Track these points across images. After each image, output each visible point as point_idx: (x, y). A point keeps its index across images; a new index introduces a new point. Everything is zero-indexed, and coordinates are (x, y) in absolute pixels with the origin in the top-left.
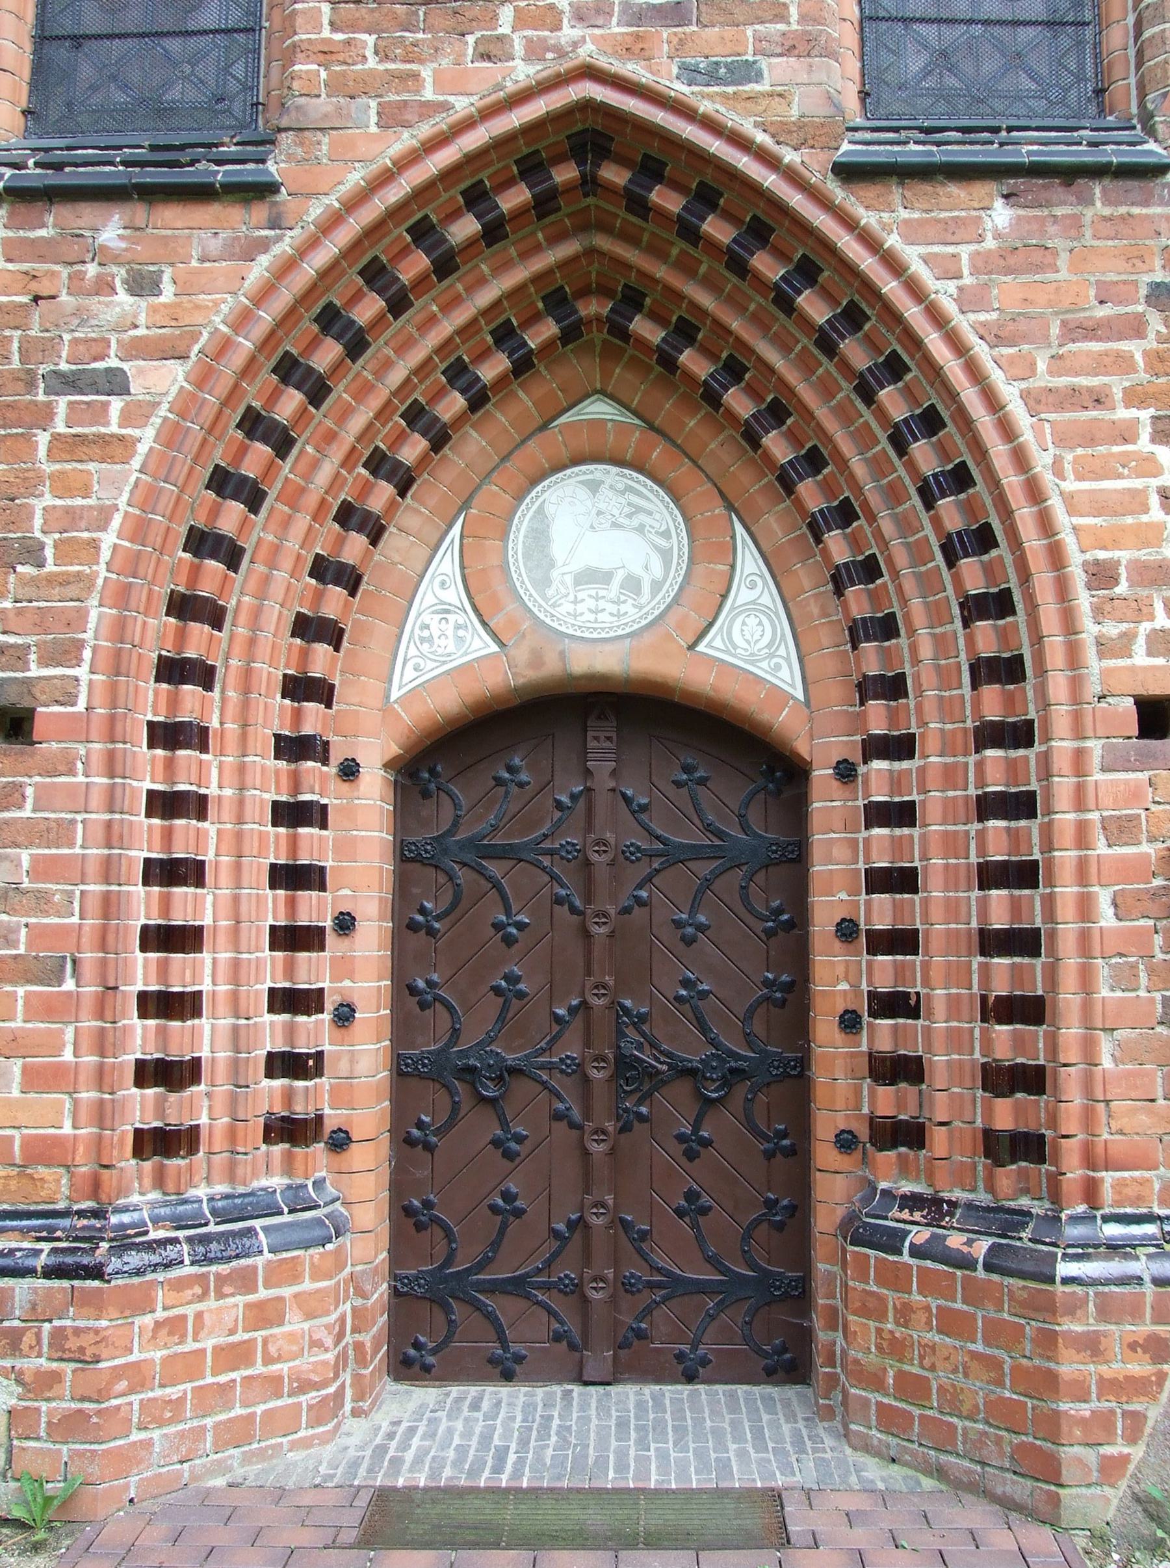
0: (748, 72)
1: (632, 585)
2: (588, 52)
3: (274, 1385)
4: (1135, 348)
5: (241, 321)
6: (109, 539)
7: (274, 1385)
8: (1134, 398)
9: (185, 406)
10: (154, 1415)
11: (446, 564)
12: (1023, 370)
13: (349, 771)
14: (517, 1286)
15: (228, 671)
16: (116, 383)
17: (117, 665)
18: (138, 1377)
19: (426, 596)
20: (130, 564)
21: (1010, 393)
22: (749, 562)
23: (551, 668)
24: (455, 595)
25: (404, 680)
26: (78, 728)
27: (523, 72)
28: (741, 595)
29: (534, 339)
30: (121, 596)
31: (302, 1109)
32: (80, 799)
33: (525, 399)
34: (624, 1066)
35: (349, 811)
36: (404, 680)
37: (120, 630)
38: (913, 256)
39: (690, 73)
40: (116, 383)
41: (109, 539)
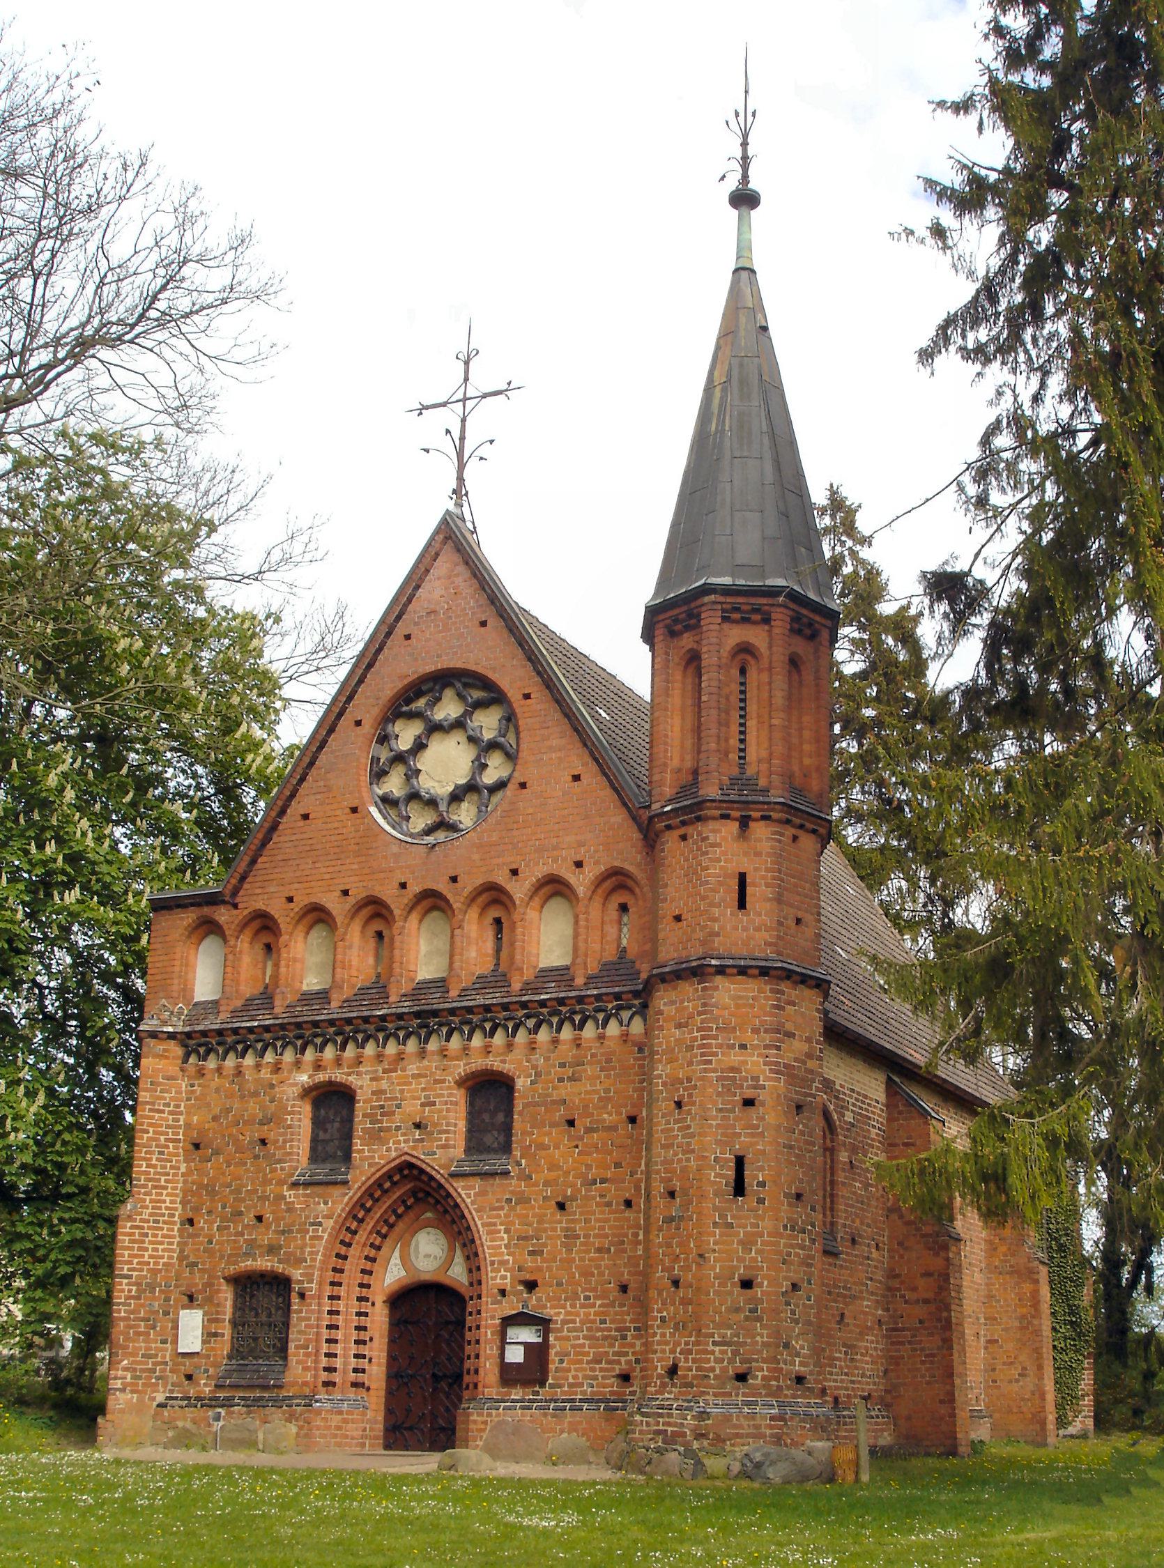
0: (435, 1153)
1: (435, 1257)
2: (406, 1149)
3: (347, 1437)
4: (502, 1213)
5: (343, 1210)
6: (319, 1257)
7: (347, 1437)
8: (501, 1224)
9: (333, 1228)
10: (322, 1436)
11: (397, 1253)
12: (481, 1218)
13: (373, 1304)
14: (410, 1429)
15: (345, 1282)
16: (320, 1224)
17: (320, 1284)
18: (318, 1428)
19: (393, 1261)
20: (323, 1262)
21: (479, 1223)
22: (458, 1252)
23: (416, 1279)
24: (398, 1261)
25: (387, 1282)
26: (312, 1297)
27: (394, 1154)
28: (456, 1260)
29: (400, 1211)
30: (321, 1269)
31: (360, 1380)
32: (312, 1311)
33: (411, 1214)
34: (434, 1375)
35: (373, 1314)
36: (387, 1282)
37: (321, 1276)
38: (463, 1193)
39: (424, 1154)
40: (320, 1224)
41: (319, 1257)
